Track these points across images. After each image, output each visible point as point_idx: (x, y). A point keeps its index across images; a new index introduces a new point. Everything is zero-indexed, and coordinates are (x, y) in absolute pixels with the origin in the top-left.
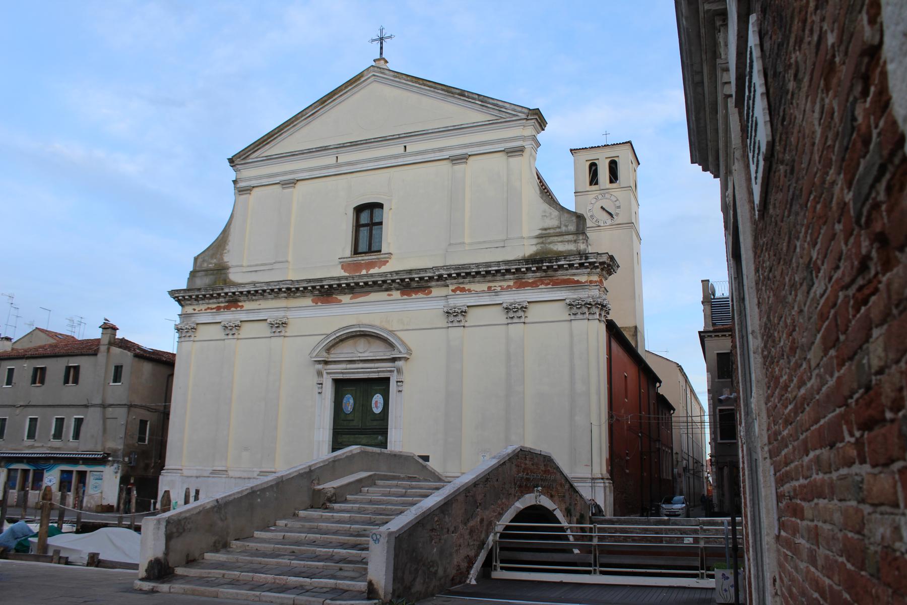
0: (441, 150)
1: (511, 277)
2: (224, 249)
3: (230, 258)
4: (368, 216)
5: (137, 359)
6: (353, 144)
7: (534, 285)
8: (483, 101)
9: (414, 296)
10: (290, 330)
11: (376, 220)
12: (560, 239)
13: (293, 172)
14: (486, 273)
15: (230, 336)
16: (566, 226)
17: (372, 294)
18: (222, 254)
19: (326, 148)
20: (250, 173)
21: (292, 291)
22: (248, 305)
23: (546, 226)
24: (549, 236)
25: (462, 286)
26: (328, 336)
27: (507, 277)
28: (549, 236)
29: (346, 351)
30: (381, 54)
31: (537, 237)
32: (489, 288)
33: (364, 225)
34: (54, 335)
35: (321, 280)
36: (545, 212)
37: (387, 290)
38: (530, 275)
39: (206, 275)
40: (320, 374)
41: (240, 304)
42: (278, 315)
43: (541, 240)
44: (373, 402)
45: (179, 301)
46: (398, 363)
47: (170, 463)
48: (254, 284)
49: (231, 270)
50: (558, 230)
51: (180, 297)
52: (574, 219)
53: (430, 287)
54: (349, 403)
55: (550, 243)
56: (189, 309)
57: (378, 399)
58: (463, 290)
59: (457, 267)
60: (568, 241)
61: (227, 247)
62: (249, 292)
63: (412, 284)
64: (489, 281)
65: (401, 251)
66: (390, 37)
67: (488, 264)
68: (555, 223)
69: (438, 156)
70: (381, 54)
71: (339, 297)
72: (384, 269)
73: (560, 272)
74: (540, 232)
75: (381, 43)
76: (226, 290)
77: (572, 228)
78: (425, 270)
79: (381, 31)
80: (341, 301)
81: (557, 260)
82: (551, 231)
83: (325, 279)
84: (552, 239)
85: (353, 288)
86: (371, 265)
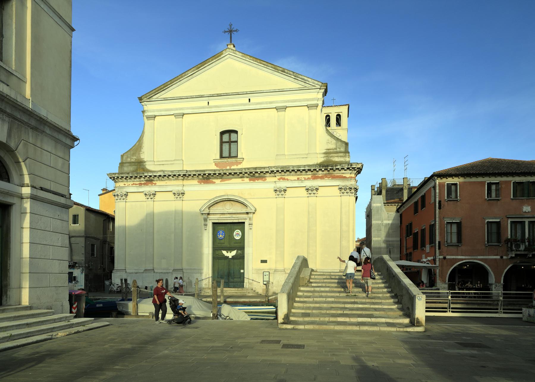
1: (310, 173)
2: (140, 151)
3: (145, 155)
4: (228, 138)
5: (88, 213)
7: (322, 178)
9: (256, 181)
10: (185, 197)
12: (336, 155)
14: (297, 171)
16: (340, 148)
18: (139, 154)
19: (202, 96)
21: (186, 176)
22: (159, 183)
23: (329, 148)
24: (330, 153)
25: (283, 177)
28: (330, 153)
31: (325, 153)
32: (298, 179)
35: (204, 171)
36: (328, 140)
37: (241, 177)
39: (131, 165)
41: (154, 182)
43: (326, 155)
47: (117, 265)
48: (163, 171)
49: (147, 163)
50: (335, 150)
52: (344, 145)
55: (331, 157)
58: (284, 179)
59: (283, 167)
60: (341, 156)
61: (142, 150)
62: (160, 176)
63: (255, 174)
65: (249, 156)
66: (236, 31)
68: (333, 146)
71: (214, 180)
72: (240, 167)
74: (325, 151)
76: (146, 174)
77: (343, 149)
78: (264, 168)
79: (231, 25)
80: (215, 183)
81: (336, 166)
82: (332, 151)
83: (207, 170)
84: (332, 155)
85: (222, 176)
86: (233, 164)
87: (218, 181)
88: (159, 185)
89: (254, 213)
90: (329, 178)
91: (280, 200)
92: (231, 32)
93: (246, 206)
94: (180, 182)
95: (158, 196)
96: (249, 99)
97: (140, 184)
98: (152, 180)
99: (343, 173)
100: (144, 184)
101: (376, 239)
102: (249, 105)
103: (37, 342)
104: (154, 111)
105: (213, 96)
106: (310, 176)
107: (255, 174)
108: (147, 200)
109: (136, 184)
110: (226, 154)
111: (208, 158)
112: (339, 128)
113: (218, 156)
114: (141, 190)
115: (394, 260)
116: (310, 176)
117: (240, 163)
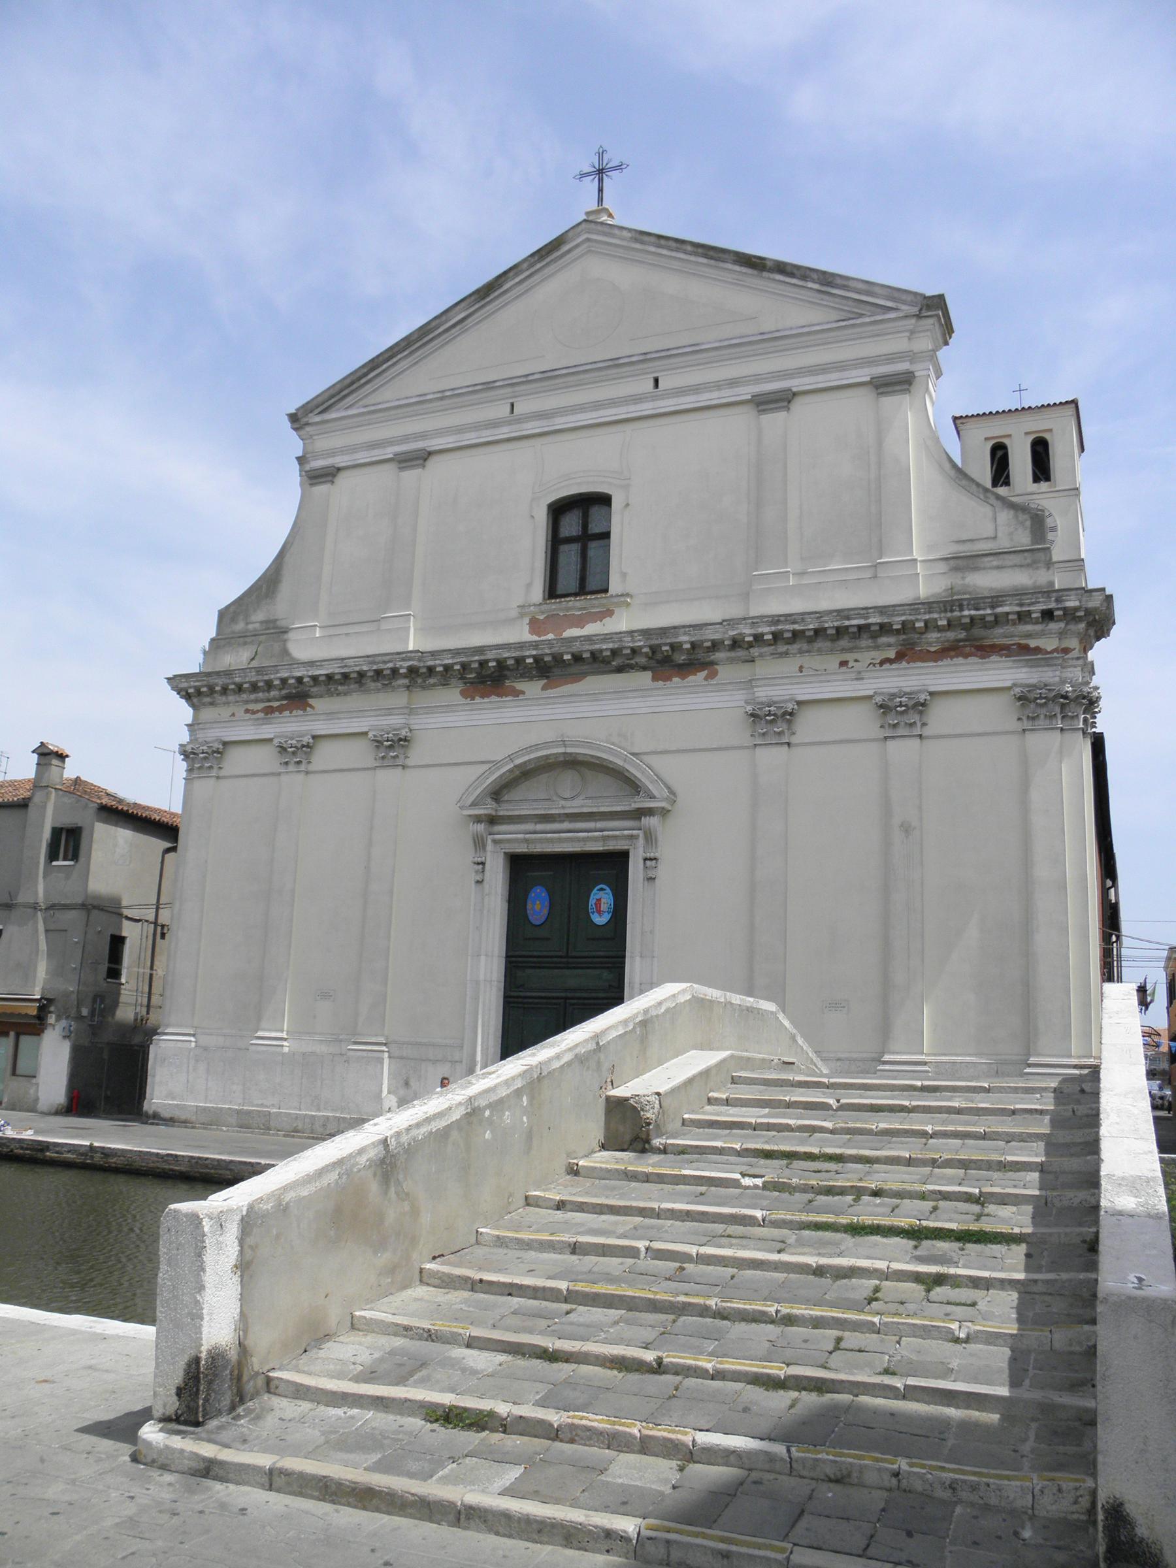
0: (733, 383)
1: (891, 640)
4: (578, 528)
6: (549, 377)
9: (676, 680)
10: (416, 755)
11: (595, 528)
13: (423, 436)
17: (589, 679)
19: (489, 386)
20: (332, 443)
26: (496, 764)
27: (884, 640)
30: (600, 200)
33: (569, 540)
38: (933, 636)
40: (479, 843)
41: (310, 701)
44: (592, 901)
45: (187, 697)
46: (646, 821)
51: (195, 690)
53: (712, 663)
54: (538, 906)
56: (208, 714)
57: (602, 898)
62: (330, 677)
63: (671, 658)
64: (843, 650)
65: (648, 589)
66: (619, 167)
67: (842, 613)
69: (727, 395)
70: (600, 200)
71: (519, 686)
72: (591, 629)
73: (999, 631)
75: (601, 181)
79: (601, 154)
80: (523, 693)
85: (551, 668)
87: (532, 688)
88: (322, 717)
89: (664, 813)
90: (966, 656)
91: (771, 757)
92: (600, 172)
93: (633, 786)
94: (397, 698)
95: (325, 756)
96: (656, 381)
97: (269, 711)
99: (1029, 636)
101: (42, 970)
102: (655, 398)
103: (945, 1055)
104: (332, 453)
105: (527, 379)
106: (891, 654)
107: (671, 658)
108: (282, 769)
109: (254, 712)
110: (568, 578)
111: (503, 604)
112: (1044, 486)
113: (537, 592)
114: (267, 731)
115: (427, 1476)
116: (891, 654)
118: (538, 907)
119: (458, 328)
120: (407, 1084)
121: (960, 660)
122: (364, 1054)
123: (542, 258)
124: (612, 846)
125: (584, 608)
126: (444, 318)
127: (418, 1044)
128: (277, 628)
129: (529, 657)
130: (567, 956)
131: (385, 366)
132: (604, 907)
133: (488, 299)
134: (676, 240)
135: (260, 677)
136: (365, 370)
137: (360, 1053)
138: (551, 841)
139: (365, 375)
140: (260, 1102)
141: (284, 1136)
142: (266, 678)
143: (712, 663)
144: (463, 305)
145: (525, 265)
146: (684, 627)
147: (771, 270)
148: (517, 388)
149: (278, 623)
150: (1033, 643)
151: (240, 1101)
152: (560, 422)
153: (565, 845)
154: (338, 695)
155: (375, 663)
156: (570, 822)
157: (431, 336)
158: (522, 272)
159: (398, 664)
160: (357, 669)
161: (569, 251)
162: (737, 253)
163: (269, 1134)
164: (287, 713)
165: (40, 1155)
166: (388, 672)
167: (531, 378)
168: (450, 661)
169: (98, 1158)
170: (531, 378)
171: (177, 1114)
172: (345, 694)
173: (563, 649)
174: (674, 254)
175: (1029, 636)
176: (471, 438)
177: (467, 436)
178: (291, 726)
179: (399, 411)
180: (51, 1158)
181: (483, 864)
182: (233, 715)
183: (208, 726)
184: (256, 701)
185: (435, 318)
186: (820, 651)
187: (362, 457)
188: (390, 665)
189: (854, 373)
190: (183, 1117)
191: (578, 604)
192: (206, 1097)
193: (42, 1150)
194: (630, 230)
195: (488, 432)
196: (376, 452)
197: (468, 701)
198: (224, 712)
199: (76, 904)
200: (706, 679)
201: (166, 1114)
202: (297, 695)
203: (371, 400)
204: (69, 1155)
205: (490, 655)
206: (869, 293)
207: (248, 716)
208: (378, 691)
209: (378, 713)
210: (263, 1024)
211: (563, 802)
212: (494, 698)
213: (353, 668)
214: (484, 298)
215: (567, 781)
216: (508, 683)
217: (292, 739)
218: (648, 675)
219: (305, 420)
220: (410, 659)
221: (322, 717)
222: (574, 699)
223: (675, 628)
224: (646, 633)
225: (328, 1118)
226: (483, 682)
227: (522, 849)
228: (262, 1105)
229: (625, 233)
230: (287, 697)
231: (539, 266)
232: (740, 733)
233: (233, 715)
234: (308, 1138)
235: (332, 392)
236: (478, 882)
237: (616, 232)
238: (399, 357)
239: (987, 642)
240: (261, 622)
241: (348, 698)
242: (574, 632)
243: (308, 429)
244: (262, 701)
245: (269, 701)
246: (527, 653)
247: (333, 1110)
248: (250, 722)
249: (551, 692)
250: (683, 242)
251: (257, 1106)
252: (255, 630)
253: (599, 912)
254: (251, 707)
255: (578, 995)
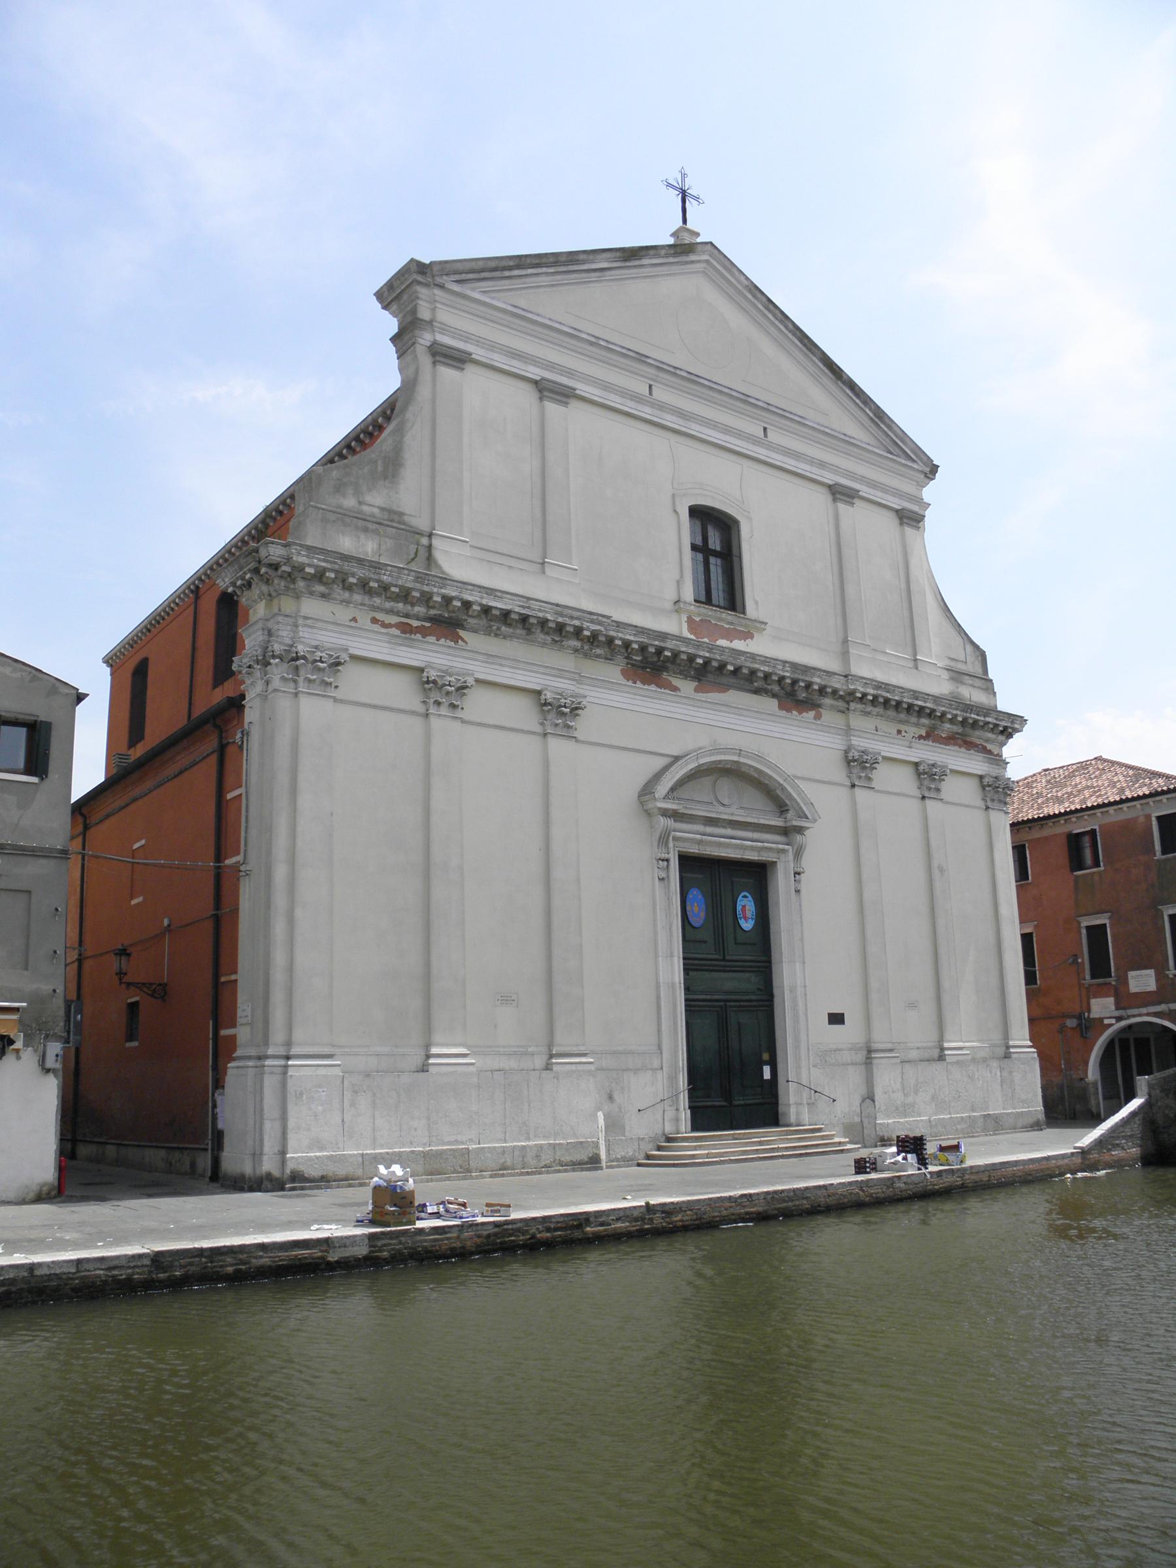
0: (822, 465)
6: (692, 379)
8: (879, 416)
9: (639, 684)
10: (585, 726)
13: (570, 373)
15: (444, 710)
17: (731, 692)
19: (641, 358)
29: (700, 801)
30: (685, 221)
34: (1140, 773)
40: (664, 840)
41: (462, 633)
42: (556, 686)
44: (739, 908)
62: (506, 614)
63: (796, 692)
64: (901, 722)
67: (916, 694)
70: (685, 221)
71: (676, 682)
72: (738, 645)
80: (675, 689)
86: (730, 635)
87: (687, 687)
88: (466, 657)
94: (564, 660)
98: (459, 624)
99: (987, 741)
100: (418, 630)
107: (796, 692)
111: (655, 593)
117: (747, 635)
118: (696, 909)
119: (597, 274)
120: (611, 1098)
121: (957, 748)
122: (573, 1067)
123: (675, 254)
124: (753, 856)
125: (732, 623)
126: (591, 257)
127: (614, 1053)
128: (404, 524)
129: (700, 657)
130: (724, 960)
131: (530, 271)
132: (749, 914)
133: (628, 264)
134: (782, 313)
135: (418, 586)
136: (511, 263)
137: (568, 1067)
138: (720, 845)
139: (510, 268)
140: (453, 1138)
141: (491, 1176)
142: (426, 588)
143: (819, 706)
144: (608, 255)
145: (663, 252)
146: (820, 670)
147: (844, 383)
148: (661, 374)
149: (406, 518)
150: (989, 747)
151: (426, 1140)
152: (695, 429)
153: (729, 850)
154: (496, 635)
155: (561, 615)
156: (733, 828)
157: (576, 268)
158: (659, 256)
159: (586, 625)
160: (541, 615)
161: (693, 262)
162: (823, 353)
163: (471, 1178)
164: (432, 639)
165: (577, 1234)
166: (571, 629)
167: (678, 372)
168: (632, 638)
169: (658, 1220)
170: (678, 372)
171: (331, 1169)
172: (505, 638)
173: (730, 660)
174: (777, 322)
175: (987, 741)
176: (615, 400)
177: (612, 397)
178: (433, 655)
179: (546, 332)
180: (593, 1233)
181: (667, 860)
182: (354, 619)
183: (319, 625)
184: (390, 612)
185: (584, 252)
186: (888, 717)
187: (499, 360)
188: (577, 623)
189: (890, 498)
190: (342, 1172)
191: (730, 618)
192: (375, 1140)
193: (579, 1226)
194: (747, 278)
195: (632, 404)
196: (515, 363)
197: (630, 683)
198: (343, 614)
199: (51, 850)
200: (815, 718)
201: (314, 1172)
202: (448, 619)
203: (523, 300)
204: (619, 1225)
205: (670, 644)
206: (902, 441)
207: (376, 627)
208: (544, 645)
209: (548, 671)
210: (437, 1037)
211: (722, 809)
212: (653, 687)
213: (536, 612)
214: (625, 261)
215: (725, 787)
216: (665, 675)
217: (451, 676)
218: (775, 702)
219: (438, 280)
220: (600, 623)
221: (480, 657)
222: (724, 708)
223: (814, 669)
224: (795, 666)
225: (541, 1147)
226: (644, 668)
227: (694, 850)
228: (457, 1142)
229: (742, 278)
230: (434, 620)
231: (671, 260)
232: (839, 773)
233: (354, 619)
234: (522, 1174)
235: (473, 265)
236: (661, 879)
237: (737, 273)
238: (544, 270)
239: (968, 739)
240: (382, 509)
241: (508, 643)
242: (722, 642)
243: (437, 291)
244: (398, 614)
245: (407, 616)
246: (701, 653)
247: (545, 1137)
248: (386, 638)
249: (700, 696)
250: (787, 317)
251: (449, 1143)
252: (373, 515)
253: (746, 918)
254: (380, 616)
255: (734, 997)
